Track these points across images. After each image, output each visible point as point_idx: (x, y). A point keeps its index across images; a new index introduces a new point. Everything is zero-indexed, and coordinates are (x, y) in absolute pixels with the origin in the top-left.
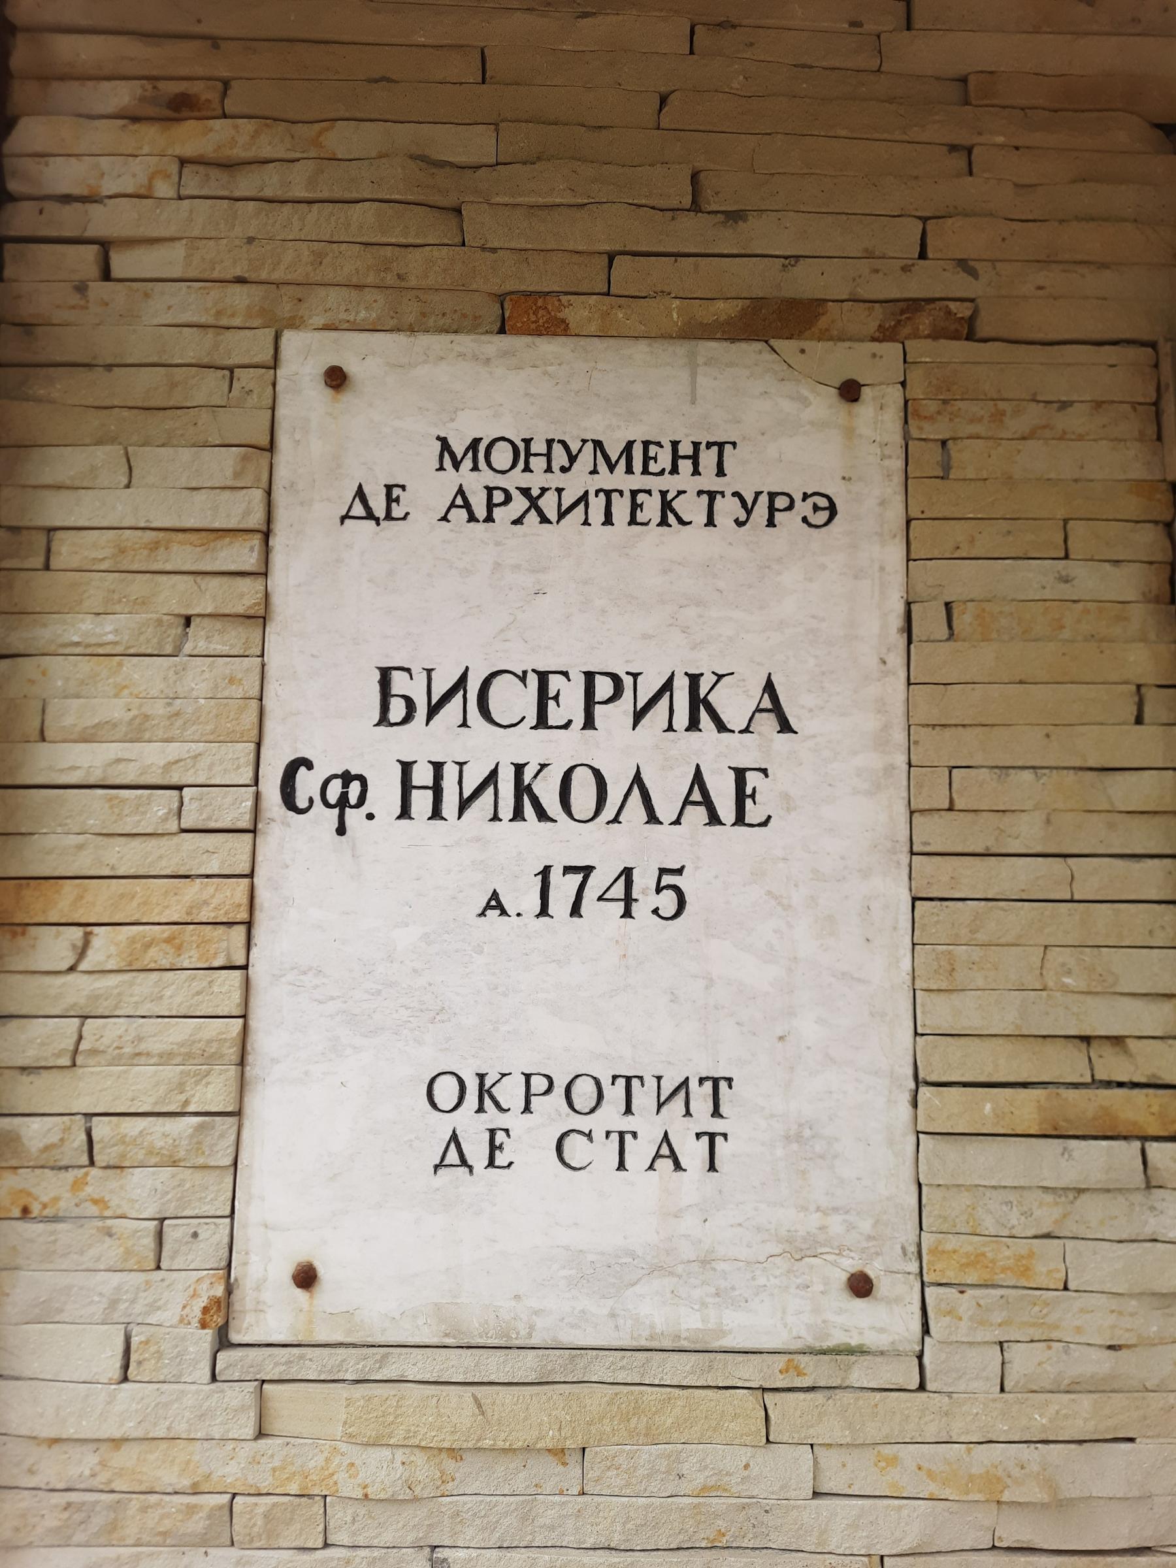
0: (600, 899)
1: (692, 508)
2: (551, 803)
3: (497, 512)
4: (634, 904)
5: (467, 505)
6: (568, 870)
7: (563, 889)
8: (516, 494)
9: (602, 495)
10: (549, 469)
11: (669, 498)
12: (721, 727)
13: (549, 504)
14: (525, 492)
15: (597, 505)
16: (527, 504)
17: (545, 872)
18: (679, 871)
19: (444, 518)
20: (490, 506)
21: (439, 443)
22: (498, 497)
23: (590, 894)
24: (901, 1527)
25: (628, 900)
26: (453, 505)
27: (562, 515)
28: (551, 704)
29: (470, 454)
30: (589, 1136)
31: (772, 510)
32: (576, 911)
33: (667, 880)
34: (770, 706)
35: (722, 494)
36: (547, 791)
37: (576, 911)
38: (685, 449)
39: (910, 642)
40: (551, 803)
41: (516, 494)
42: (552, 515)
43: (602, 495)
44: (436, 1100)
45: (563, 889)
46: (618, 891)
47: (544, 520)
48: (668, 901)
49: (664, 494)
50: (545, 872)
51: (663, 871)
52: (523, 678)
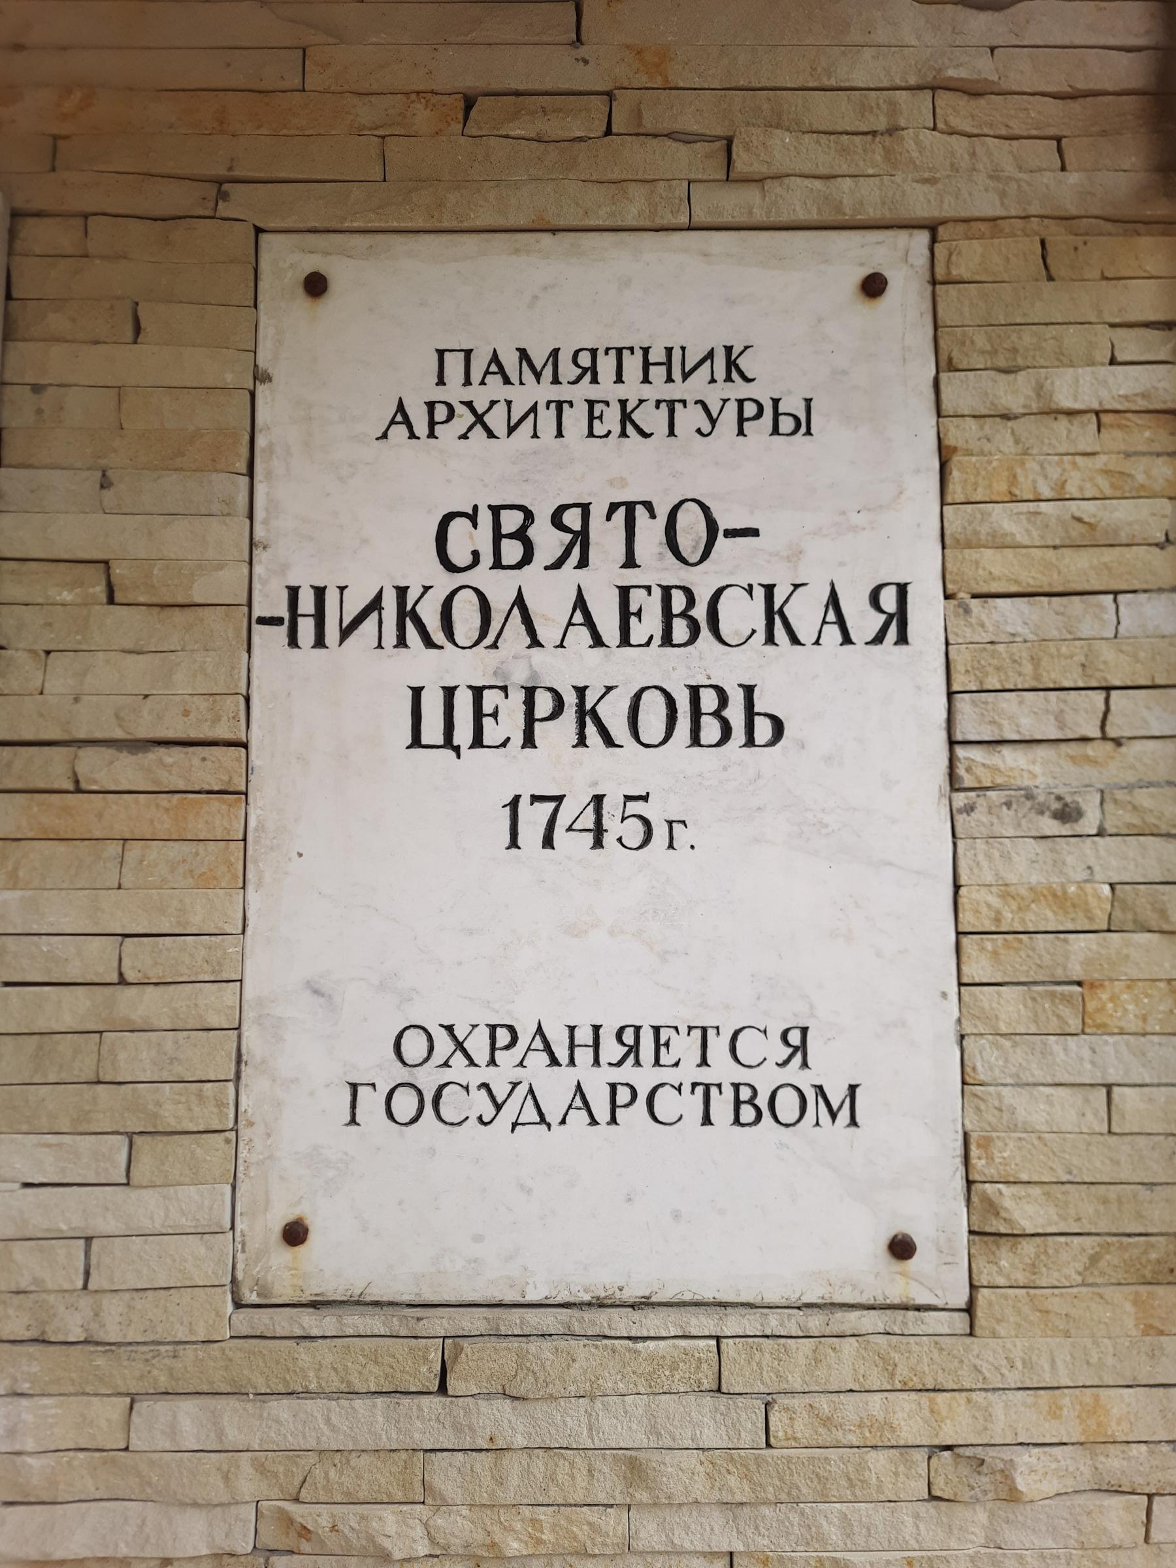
0: (570, 829)
1: (652, 419)
2: (619, 729)
3: (438, 429)
4: (605, 834)
5: (407, 422)
6: (535, 799)
7: (533, 818)
8: (460, 409)
9: (663, 405)
10: (670, 379)
11: (629, 410)
12: (795, 640)
13: (497, 420)
14: (469, 405)
15: (547, 418)
16: (473, 419)
17: (514, 803)
18: (645, 798)
19: (385, 436)
20: (432, 424)
21: (518, 354)
22: (441, 413)
23: (563, 821)
24: (193, 1535)
25: (599, 832)
26: (393, 422)
27: (511, 430)
28: (633, 620)
29: (524, 364)
30: (467, 1089)
31: (741, 420)
32: (548, 842)
33: (634, 807)
34: (834, 619)
35: (684, 402)
36: (614, 714)
37: (548, 842)
38: (657, 355)
39: (943, 548)
40: (619, 729)
41: (460, 409)
42: (500, 428)
43: (663, 405)
44: (403, 1049)
45: (533, 818)
46: (588, 820)
47: (491, 435)
48: (634, 831)
49: (623, 403)
50: (514, 803)
51: (628, 798)
52: (750, 590)
